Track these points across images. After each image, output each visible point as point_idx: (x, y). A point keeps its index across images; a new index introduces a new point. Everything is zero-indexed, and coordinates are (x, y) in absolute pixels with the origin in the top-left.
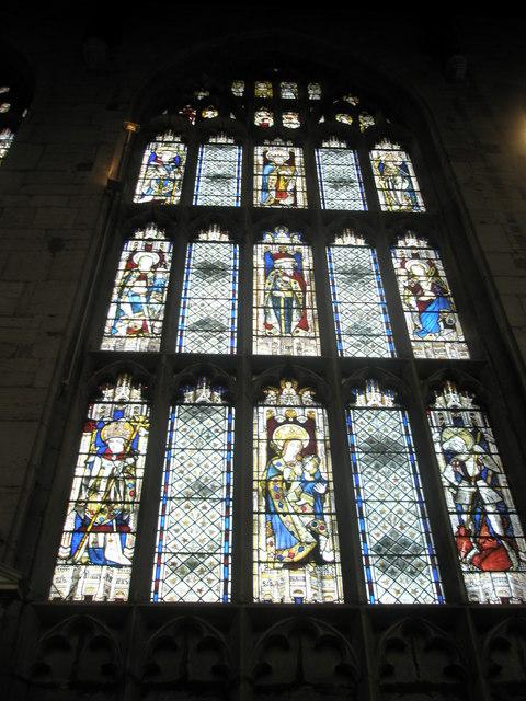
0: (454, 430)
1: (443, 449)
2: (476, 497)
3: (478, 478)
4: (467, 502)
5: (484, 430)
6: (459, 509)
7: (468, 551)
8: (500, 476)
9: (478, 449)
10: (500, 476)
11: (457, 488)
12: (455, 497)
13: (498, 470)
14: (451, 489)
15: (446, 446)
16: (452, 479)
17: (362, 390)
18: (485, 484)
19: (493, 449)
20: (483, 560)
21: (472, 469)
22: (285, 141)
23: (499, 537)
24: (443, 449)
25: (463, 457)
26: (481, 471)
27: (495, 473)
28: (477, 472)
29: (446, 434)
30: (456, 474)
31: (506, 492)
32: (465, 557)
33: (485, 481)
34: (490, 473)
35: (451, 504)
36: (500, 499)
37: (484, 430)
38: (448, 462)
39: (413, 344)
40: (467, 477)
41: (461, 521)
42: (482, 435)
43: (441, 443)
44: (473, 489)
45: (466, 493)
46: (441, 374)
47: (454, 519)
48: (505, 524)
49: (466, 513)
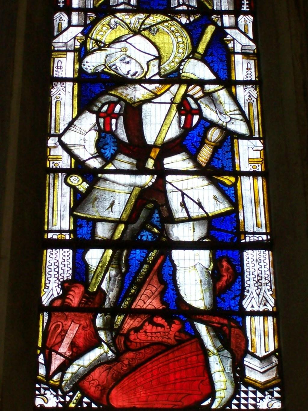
0: (134, 20)
1: (81, 71)
2: (151, 204)
3: (169, 148)
4: (116, 214)
5: (227, 20)
6: (84, 232)
7: (78, 352)
8: (243, 145)
9: (198, 70)
10: (243, 145)
11: (92, 176)
12: (79, 200)
13: (241, 128)
14: (75, 180)
15: (94, 62)
16: (87, 151)
17: (218, 240)
18: (189, 166)
19: (243, 69)
20: (118, 380)
21: (159, 122)
22: (125, 283)
23: (194, 314)
24: (81, 71)
25: (139, 93)
26: (187, 129)
27: (229, 137)
28: (174, 132)
29: (103, 32)
30: (104, 137)
31: (251, 190)
32: (63, 368)
33: (193, 157)
34: (214, 135)
35: (59, 217)
36: (224, 207)
37: (227, 20)
38: (84, 104)
39: (77, 187)
40: (137, 148)
41: (80, 268)
42: (220, 32)
43: (82, 53)
44: (146, 180)
45: (119, 191)
46: (90, 38)
47: (58, 264)
48: (226, 280)
49: (103, 244)
